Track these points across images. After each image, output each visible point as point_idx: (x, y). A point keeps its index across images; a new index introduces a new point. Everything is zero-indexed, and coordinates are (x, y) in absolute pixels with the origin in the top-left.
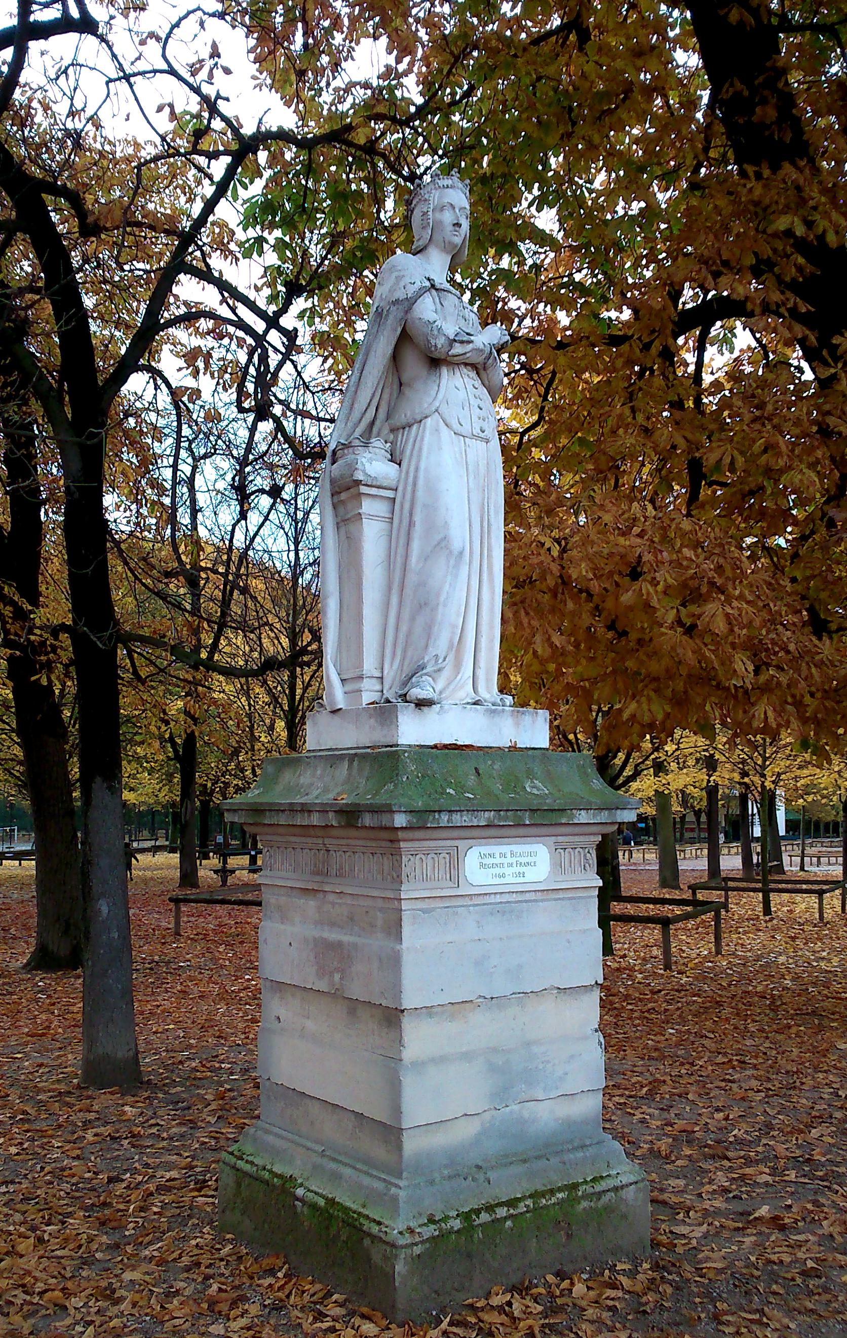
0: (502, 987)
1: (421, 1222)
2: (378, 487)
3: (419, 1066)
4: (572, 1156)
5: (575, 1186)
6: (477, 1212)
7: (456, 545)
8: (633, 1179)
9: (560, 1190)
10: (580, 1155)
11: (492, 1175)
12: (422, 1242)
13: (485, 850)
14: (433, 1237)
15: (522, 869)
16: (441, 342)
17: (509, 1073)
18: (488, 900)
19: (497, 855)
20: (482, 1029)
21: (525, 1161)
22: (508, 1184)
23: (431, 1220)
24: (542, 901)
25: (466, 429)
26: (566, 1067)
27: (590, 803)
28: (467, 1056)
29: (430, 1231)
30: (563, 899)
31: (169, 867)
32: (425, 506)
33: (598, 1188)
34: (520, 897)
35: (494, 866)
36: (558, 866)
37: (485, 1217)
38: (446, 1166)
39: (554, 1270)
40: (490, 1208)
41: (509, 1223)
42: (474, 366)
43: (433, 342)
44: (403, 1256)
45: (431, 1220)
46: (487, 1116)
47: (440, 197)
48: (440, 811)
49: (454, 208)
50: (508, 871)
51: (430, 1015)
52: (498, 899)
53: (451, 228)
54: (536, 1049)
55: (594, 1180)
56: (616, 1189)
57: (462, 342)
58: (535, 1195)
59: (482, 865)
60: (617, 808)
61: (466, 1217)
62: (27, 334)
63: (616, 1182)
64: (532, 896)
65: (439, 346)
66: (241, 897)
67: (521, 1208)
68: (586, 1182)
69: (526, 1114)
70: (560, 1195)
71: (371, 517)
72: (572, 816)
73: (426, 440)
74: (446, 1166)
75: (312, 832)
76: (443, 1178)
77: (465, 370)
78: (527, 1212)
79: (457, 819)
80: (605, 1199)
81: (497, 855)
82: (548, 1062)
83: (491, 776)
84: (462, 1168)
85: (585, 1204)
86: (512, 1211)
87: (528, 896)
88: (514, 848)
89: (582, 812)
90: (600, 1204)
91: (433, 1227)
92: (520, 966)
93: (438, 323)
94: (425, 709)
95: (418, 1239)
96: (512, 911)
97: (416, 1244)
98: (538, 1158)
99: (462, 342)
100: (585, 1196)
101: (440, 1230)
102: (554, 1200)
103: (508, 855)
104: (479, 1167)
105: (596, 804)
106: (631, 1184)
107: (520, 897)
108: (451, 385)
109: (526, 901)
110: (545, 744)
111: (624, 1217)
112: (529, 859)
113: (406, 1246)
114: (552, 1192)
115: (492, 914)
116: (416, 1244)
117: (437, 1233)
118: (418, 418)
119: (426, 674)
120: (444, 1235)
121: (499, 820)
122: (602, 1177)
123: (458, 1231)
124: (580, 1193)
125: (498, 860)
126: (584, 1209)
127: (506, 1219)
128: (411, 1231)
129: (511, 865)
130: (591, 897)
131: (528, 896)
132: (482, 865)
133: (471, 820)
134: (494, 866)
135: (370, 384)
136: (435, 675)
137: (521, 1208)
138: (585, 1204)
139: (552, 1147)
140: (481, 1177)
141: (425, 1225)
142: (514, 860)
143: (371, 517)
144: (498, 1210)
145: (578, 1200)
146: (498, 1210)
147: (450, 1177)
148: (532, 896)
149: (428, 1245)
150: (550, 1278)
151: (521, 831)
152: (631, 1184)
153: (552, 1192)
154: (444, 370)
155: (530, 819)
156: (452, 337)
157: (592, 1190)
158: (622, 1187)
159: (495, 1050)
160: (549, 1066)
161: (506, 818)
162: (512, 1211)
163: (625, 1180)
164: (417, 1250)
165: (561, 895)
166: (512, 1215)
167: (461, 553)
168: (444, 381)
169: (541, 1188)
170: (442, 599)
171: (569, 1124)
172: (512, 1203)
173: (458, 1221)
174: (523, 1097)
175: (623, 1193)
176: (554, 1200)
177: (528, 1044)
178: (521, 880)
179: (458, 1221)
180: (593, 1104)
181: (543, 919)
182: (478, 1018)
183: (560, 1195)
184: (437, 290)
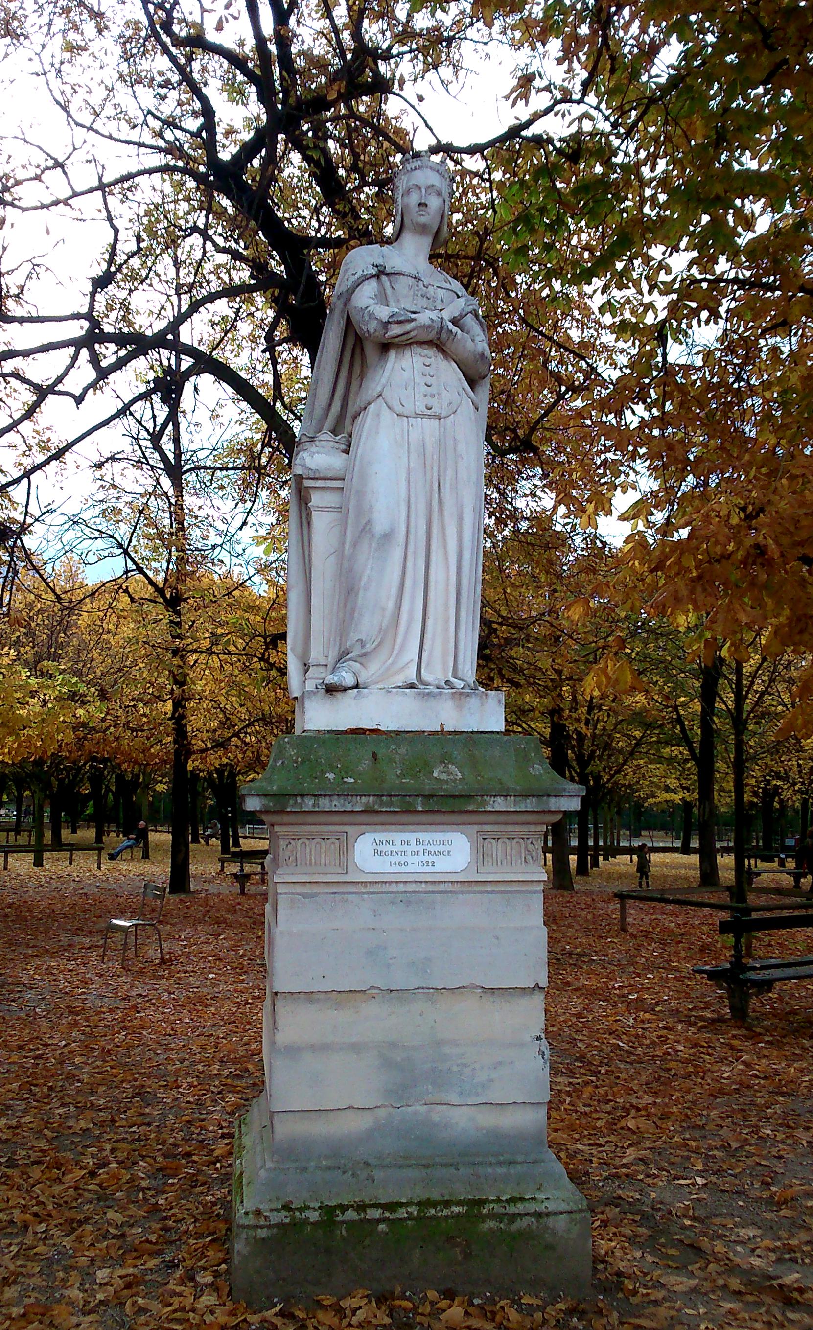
0: (401, 979)
1: (273, 1206)
2: (325, 479)
3: (293, 1051)
4: (490, 1170)
5: (481, 1203)
6: (344, 1208)
7: (380, 526)
8: (563, 1207)
9: (459, 1203)
11: (378, 1174)
12: (269, 1227)
13: (380, 836)
14: (284, 1224)
15: (431, 858)
16: (372, 326)
17: (408, 1073)
19: (398, 842)
20: (375, 1022)
21: (426, 1166)
22: (401, 1187)
23: (286, 1207)
24: (462, 893)
25: (408, 409)
26: (496, 1074)
27: (508, 789)
28: (356, 1048)
29: (282, 1217)
30: (492, 892)
31: (690, 867)
32: (357, 492)
33: (512, 1209)
34: (431, 888)
36: (480, 855)
37: (351, 1215)
38: (326, 1157)
39: (442, 1287)
40: (361, 1207)
41: (382, 1227)
42: (429, 343)
43: (365, 328)
44: (244, 1236)
45: (286, 1207)
46: (382, 1113)
47: (408, 181)
48: (302, 796)
49: (420, 188)
50: (411, 859)
52: (402, 888)
53: (417, 209)
54: (447, 1050)
55: (512, 1200)
56: (539, 1215)
57: (399, 322)
58: (425, 1204)
59: (376, 852)
60: (549, 796)
61: (329, 1211)
63: (541, 1208)
64: (449, 887)
65: (372, 331)
66: (679, 897)
67: (402, 1213)
68: (499, 1201)
69: (436, 1118)
70: (456, 1209)
71: (322, 509)
72: (486, 803)
73: (367, 425)
74: (326, 1157)
76: (318, 1167)
77: (419, 350)
78: (408, 1219)
79: (325, 804)
81: (398, 842)
82: (465, 1065)
83: (391, 760)
84: (339, 1159)
85: (491, 1224)
86: (387, 1215)
87: (442, 887)
88: (421, 836)
90: (514, 1227)
91: (284, 1213)
93: (371, 309)
94: (339, 695)
95: (262, 1222)
97: (262, 1227)
98: (445, 1165)
99: (399, 322)
100: (492, 1216)
101: (293, 1218)
102: (446, 1212)
103: (413, 842)
104: (367, 1164)
105: (516, 790)
106: (562, 1213)
107: (431, 888)
108: (397, 366)
110: (501, 726)
111: (550, 1247)
112: (441, 848)
113: (248, 1227)
114: (447, 1204)
115: (393, 903)
116: (262, 1227)
117: (287, 1221)
118: (363, 405)
119: (350, 659)
120: (296, 1225)
121: (381, 805)
123: (315, 1224)
124: (485, 1211)
125: (398, 847)
126: (491, 1229)
127: (379, 1221)
128: (258, 1213)
130: (536, 892)
131: (442, 887)
132: (376, 852)
133: (344, 805)
135: (326, 380)
136: (363, 660)
137: (402, 1213)
138: (491, 1224)
140: (363, 1175)
141: (278, 1210)
142: (420, 848)
143: (322, 509)
144: (368, 1211)
145: (483, 1218)
146: (368, 1211)
147: (329, 1168)
148: (449, 887)
149: (275, 1230)
150: (432, 1294)
152: (562, 1213)
153: (447, 1204)
154: (392, 354)
155: (423, 804)
156: (385, 319)
158: (548, 1215)
159: (393, 1045)
160: (466, 1070)
161: (391, 804)
162: (387, 1215)
163: (552, 1206)
164: (262, 1233)
165: (489, 888)
166: (388, 1219)
167: (387, 537)
168: (389, 365)
169: (435, 1196)
170: (362, 583)
171: (496, 1136)
172: (392, 1207)
173: (317, 1213)
174: (430, 1098)
175: (551, 1221)
176: (446, 1212)
177: (439, 1043)
178: (430, 869)
179: (317, 1213)
180: (533, 1119)
181: (464, 912)
182: (371, 1009)
183: (456, 1209)
184: (387, 274)
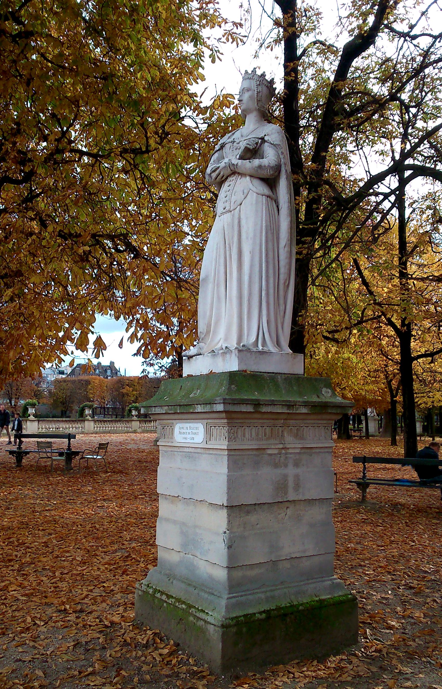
10: (206, 596)
15: (193, 436)
18: (181, 450)
28: (175, 522)
35: (184, 433)
36: (209, 434)
51: (166, 498)
56: (206, 622)
59: (180, 433)
61: (155, 591)
62: (434, 178)
64: (199, 450)
75: (297, 417)
80: (201, 623)
87: (199, 450)
88: (192, 425)
89: (199, 406)
92: (192, 485)
94: (191, 359)
96: (192, 457)
106: (213, 625)
109: (198, 453)
122: (204, 612)
129: (189, 433)
130: (224, 455)
132: (180, 433)
134: (184, 433)
139: (194, 583)
142: (190, 431)
151: (176, 416)
152: (213, 625)
157: (195, 613)
161: (171, 410)
165: (211, 452)
177: (196, 527)
181: (205, 463)
